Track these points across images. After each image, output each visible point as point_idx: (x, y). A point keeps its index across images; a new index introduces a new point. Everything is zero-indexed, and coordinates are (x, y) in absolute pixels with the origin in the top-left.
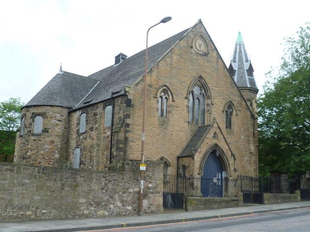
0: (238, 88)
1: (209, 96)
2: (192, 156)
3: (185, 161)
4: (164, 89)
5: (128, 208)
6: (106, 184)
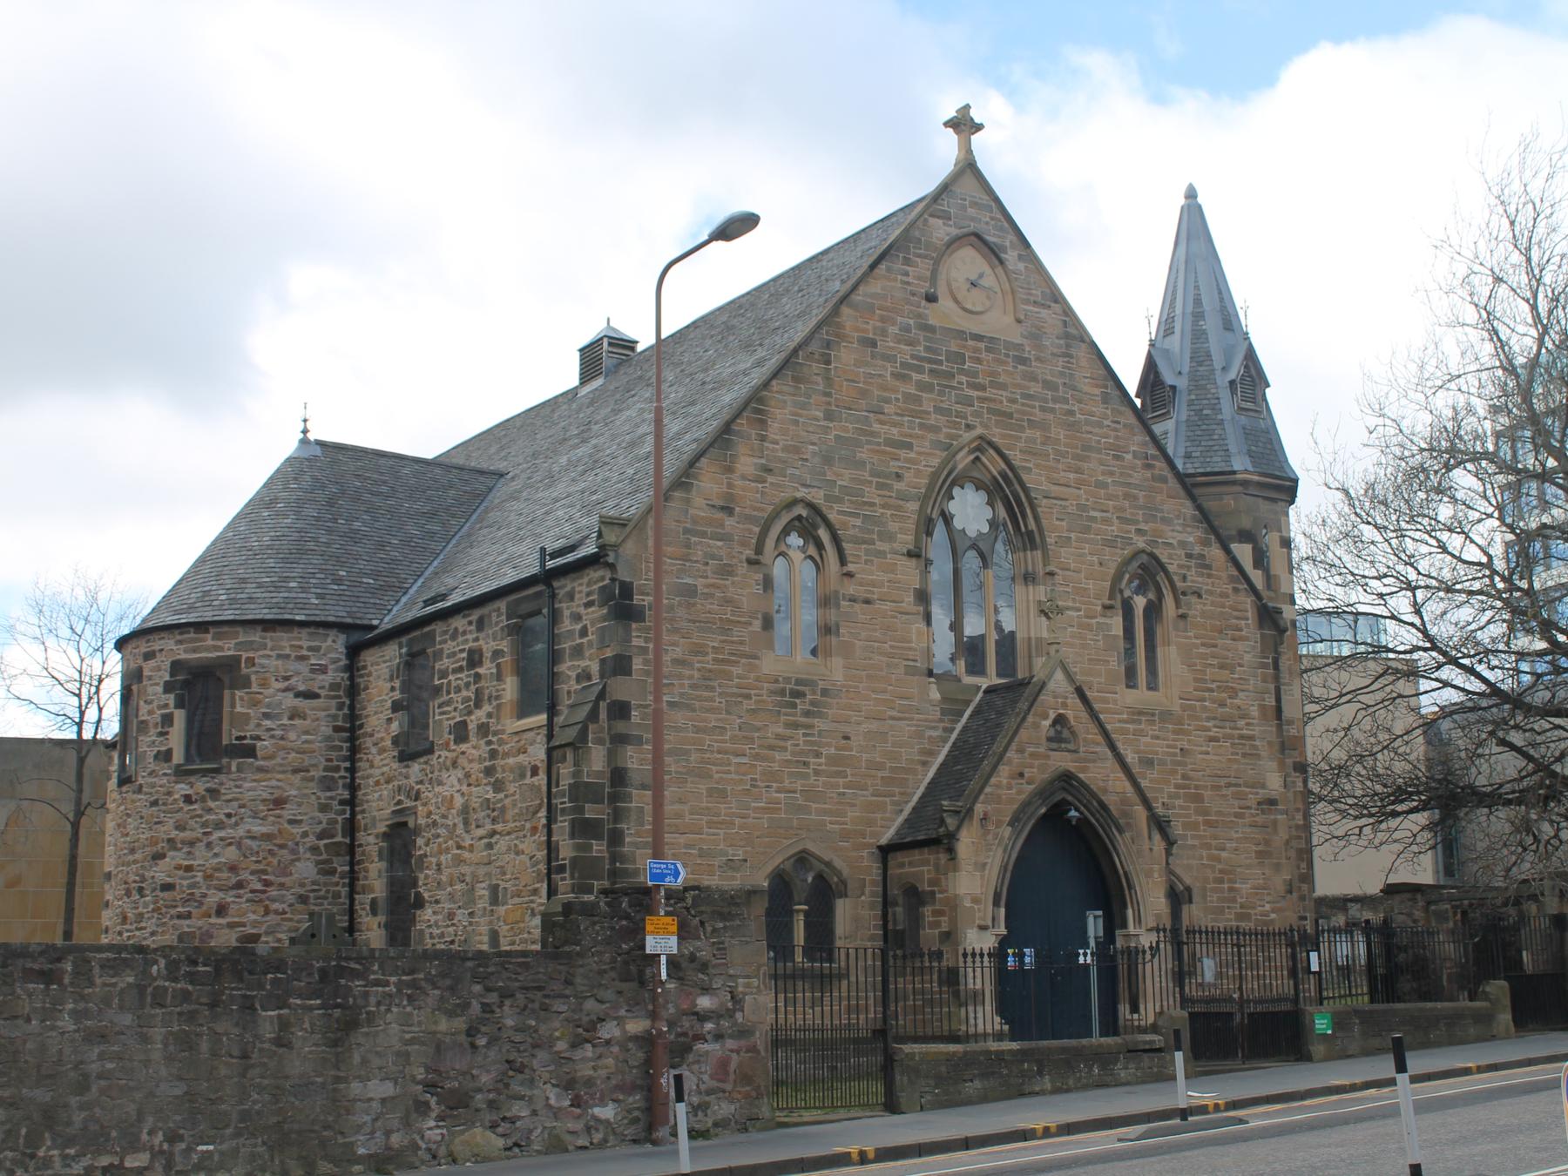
0: (1181, 478)
1: (1030, 534)
2: (943, 843)
3: (918, 867)
4: (799, 518)
5: (597, 1111)
6: (487, 1008)
